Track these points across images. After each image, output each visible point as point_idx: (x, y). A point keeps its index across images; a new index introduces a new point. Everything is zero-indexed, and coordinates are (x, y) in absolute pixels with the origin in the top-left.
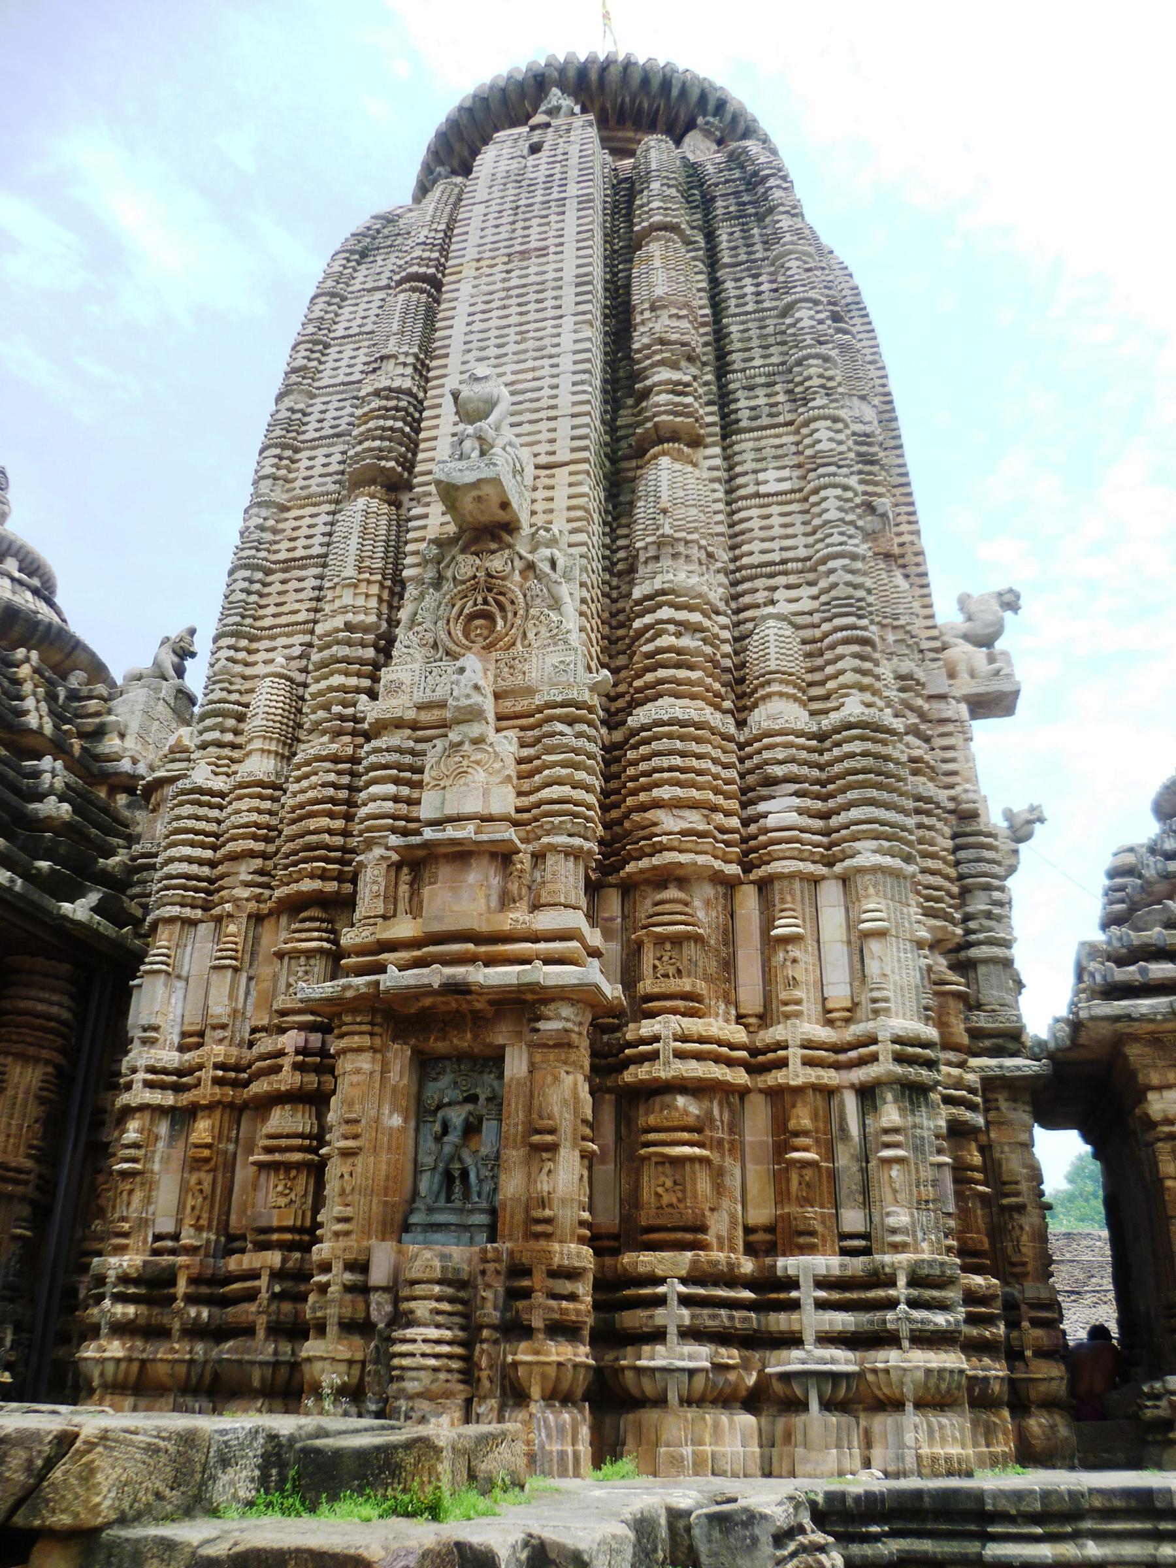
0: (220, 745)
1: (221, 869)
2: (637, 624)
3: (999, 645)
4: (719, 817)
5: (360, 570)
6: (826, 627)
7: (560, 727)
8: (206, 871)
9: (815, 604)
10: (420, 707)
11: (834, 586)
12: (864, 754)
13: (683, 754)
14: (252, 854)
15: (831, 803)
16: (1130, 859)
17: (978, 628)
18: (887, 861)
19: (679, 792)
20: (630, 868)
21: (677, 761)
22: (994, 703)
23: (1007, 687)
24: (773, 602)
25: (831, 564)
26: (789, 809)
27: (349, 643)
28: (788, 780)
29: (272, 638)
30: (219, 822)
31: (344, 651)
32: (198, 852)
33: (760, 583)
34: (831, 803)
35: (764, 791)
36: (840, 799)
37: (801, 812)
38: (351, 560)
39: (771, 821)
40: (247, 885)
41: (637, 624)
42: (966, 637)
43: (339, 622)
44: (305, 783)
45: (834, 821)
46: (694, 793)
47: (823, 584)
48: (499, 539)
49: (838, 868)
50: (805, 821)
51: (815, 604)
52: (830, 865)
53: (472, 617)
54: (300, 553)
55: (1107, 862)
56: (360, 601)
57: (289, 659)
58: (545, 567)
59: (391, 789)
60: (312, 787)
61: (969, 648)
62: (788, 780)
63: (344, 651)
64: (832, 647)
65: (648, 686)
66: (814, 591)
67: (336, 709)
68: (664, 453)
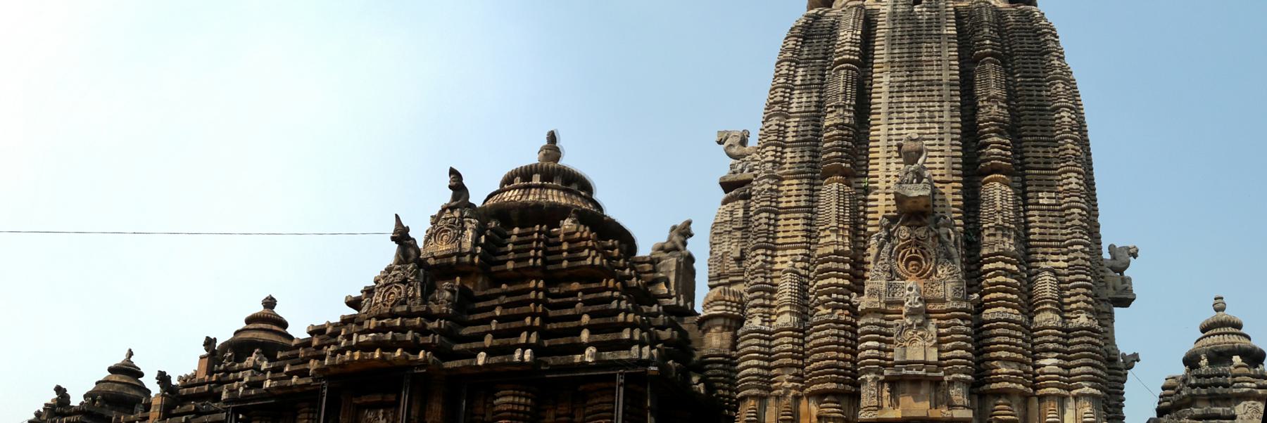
0: (763, 306)
1: (774, 372)
2: (986, 267)
3: (1126, 273)
4: (1025, 367)
5: (838, 221)
6: (1072, 277)
7: (959, 321)
8: (766, 372)
9: (1066, 265)
10: (888, 303)
11: (1076, 258)
12: (1089, 342)
13: (1010, 336)
14: (792, 366)
15: (1071, 363)
16: (1173, 382)
17: (1117, 264)
18: (1094, 391)
19: (1008, 354)
20: (986, 387)
21: (1007, 339)
22: (1125, 302)
23: (1130, 297)
24: (1045, 260)
25: (1075, 247)
26: (1054, 365)
27: (838, 261)
28: (1054, 350)
29: (785, 249)
30: (770, 347)
31: (834, 265)
32: (762, 363)
33: (1040, 250)
34: (1071, 363)
35: (1043, 355)
36: (1076, 362)
37: (1059, 366)
38: (834, 218)
39: (1046, 370)
40: (790, 381)
41: (986, 267)
42: (1111, 268)
43: (831, 249)
44: (823, 333)
45: (1073, 371)
46: (1014, 355)
47: (1071, 256)
48: (920, 220)
49: (1074, 392)
50: (1061, 370)
51: (1066, 265)
52: (1070, 389)
53: (909, 259)
54: (793, 204)
55: (1163, 382)
56: (840, 239)
57: (795, 261)
58: (945, 237)
59: (876, 344)
60: (826, 336)
61: (1112, 273)
62: (1054, 350)
63: (834, 265)
64: (1075, 287)
65: (991, 300)
66: (1066, 257)
67: (834, 296)
68: (995, 180)
